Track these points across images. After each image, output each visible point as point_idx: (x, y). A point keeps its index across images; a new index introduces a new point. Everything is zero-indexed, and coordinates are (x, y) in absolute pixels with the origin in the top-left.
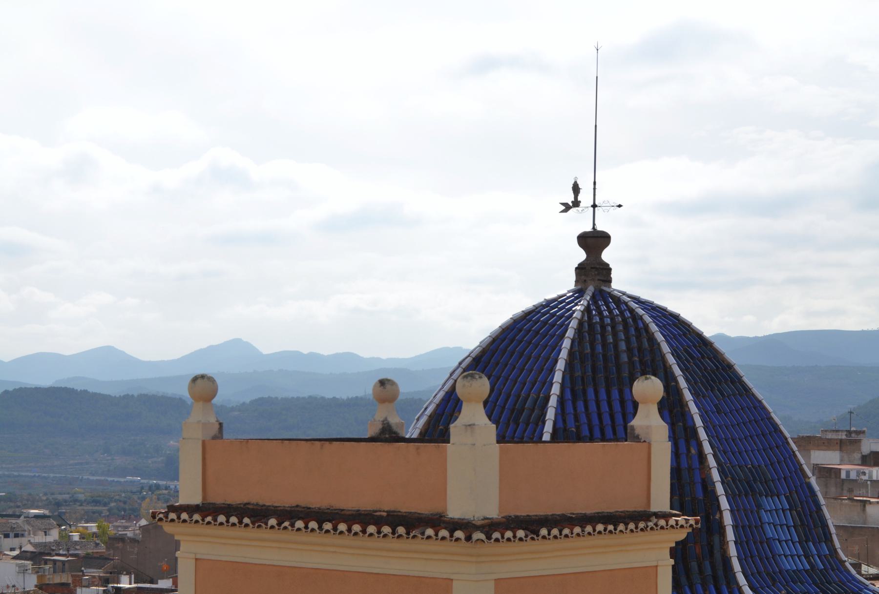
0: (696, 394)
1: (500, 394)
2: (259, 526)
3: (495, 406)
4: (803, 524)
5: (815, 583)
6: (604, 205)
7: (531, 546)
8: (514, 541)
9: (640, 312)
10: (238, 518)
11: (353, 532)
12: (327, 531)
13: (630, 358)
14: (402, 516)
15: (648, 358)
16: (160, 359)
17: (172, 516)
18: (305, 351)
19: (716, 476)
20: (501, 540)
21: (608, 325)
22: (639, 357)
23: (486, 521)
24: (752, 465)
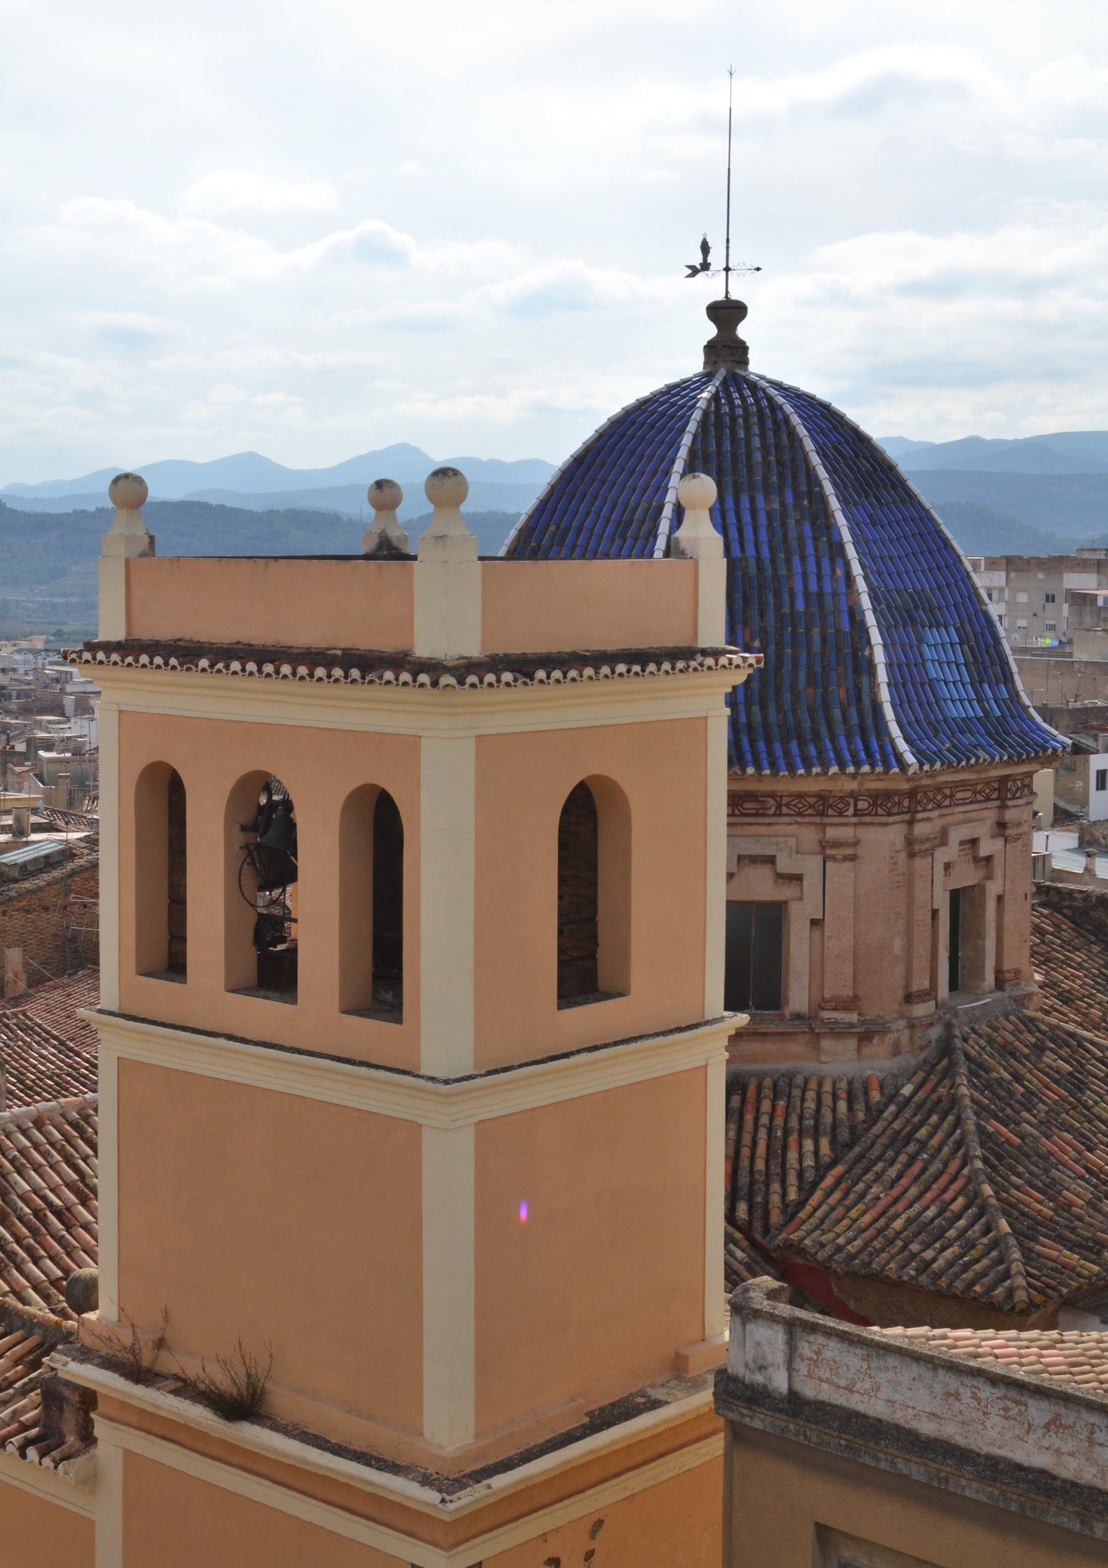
0: (845, 502)
1: (605, 502)
2: (189, 669)
3: (598, 518)
4: (976, 661)
6: (739, 268)
7: (521, 692)
8: (498, 687)
9: (781, 400)
10: (163, 658)
11: (298, 676)
12: (268, 675)
13: (765, 458)
14: (360, 655)
15: (787, 457)
16: (311, 468)
17: (87, 656)
19: (866, 602)
20: (479, 685)
21: (740, 416)
22: (776, 456)
23: (462, 661)
24: (913, 589)
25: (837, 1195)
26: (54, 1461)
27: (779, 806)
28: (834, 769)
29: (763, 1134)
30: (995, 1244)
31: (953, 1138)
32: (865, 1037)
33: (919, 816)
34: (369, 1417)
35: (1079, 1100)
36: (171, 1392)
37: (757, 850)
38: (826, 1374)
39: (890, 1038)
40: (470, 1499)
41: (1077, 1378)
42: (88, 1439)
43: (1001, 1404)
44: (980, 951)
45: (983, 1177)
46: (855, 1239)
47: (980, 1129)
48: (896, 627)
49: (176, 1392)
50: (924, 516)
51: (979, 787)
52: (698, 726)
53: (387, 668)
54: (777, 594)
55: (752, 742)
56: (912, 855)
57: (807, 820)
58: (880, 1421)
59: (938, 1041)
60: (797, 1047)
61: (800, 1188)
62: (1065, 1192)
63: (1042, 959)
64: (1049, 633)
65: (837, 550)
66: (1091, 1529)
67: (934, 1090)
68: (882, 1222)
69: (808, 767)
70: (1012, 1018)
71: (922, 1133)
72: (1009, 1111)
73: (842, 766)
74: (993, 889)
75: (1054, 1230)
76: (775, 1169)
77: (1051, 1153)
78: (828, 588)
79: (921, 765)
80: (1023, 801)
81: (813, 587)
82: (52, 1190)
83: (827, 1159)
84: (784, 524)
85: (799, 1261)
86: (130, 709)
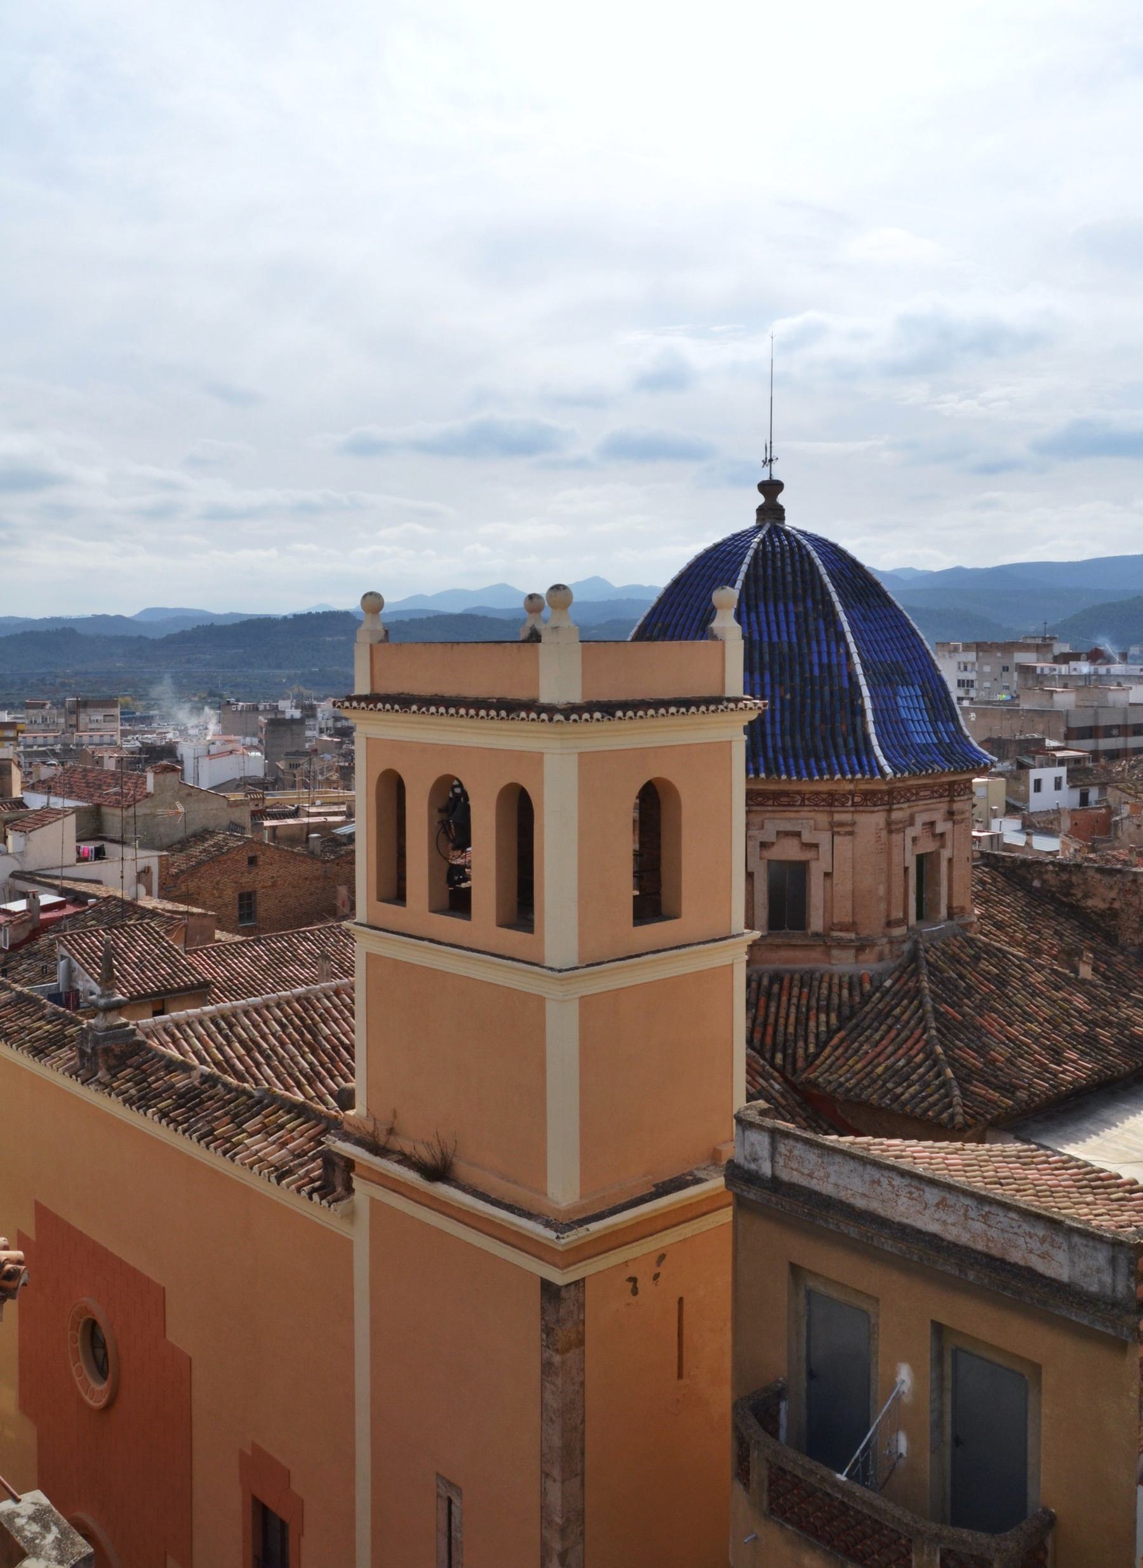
2: (406, 712)
4: (933, 707)
5: (941, 753)
7: (607, 725)
9: (805, 542)
12: (452, 715)
15: (808, 577)
17: (347, 704)
18: (646, 585)
19: (859, 670)
25: (840, 1050)
26: (328, 1202)
27: (803, 800)
28: (838, 776)
29: (793, 1009)
30: (943, 1085)
31: (917, 1015)
32: (860, 949)
33: (895, 807)
34: (515, 1182)
35: (1003, 993)
36: (396, 1162)
37: (789, 827)
38: (795, 1165)
39: (877, 949)
40: (576, 1237)
41: (968, 1174)
42: (350, 1190)
43: (907, 1190)
44: (937, 894)
45: (936, 1041)
46: (851, 1079)
47: (935, 1010)
48: (879, 686)
49: (399, 1162)
50: (898, 615)
51: (936, 788)
52: (726, 747)
53: (522, 710)
54: (801, 665)
55: (785, 759)
56: (890, 832)
57: (821, 809)
58: (830, 1197)
59: (908, 952)
60: (816, 954)
61: (817, 1045)
62: (992, 1052)
63: (981, 898)
64: (1005, 691)
65: (841, 636)
66: (966, 1275)
67: (905, 984)
68: (869, 1068)
69: (821, 773)
70: (959, 938)
71: (897, 1011)
72: (955, 998)
73: (843, 774)
74: (946, 854)
75: (983, 1077)
76: (801, 1032)
77: (982, 1026)
78: (834, 661)
79: (895, 774)
80: (965, 797)
81: (825, 660)
82: (344, 1034)
83: (834, 1027)
84: (806, 620)
85: (815, 1091)
86: (373, 736)
